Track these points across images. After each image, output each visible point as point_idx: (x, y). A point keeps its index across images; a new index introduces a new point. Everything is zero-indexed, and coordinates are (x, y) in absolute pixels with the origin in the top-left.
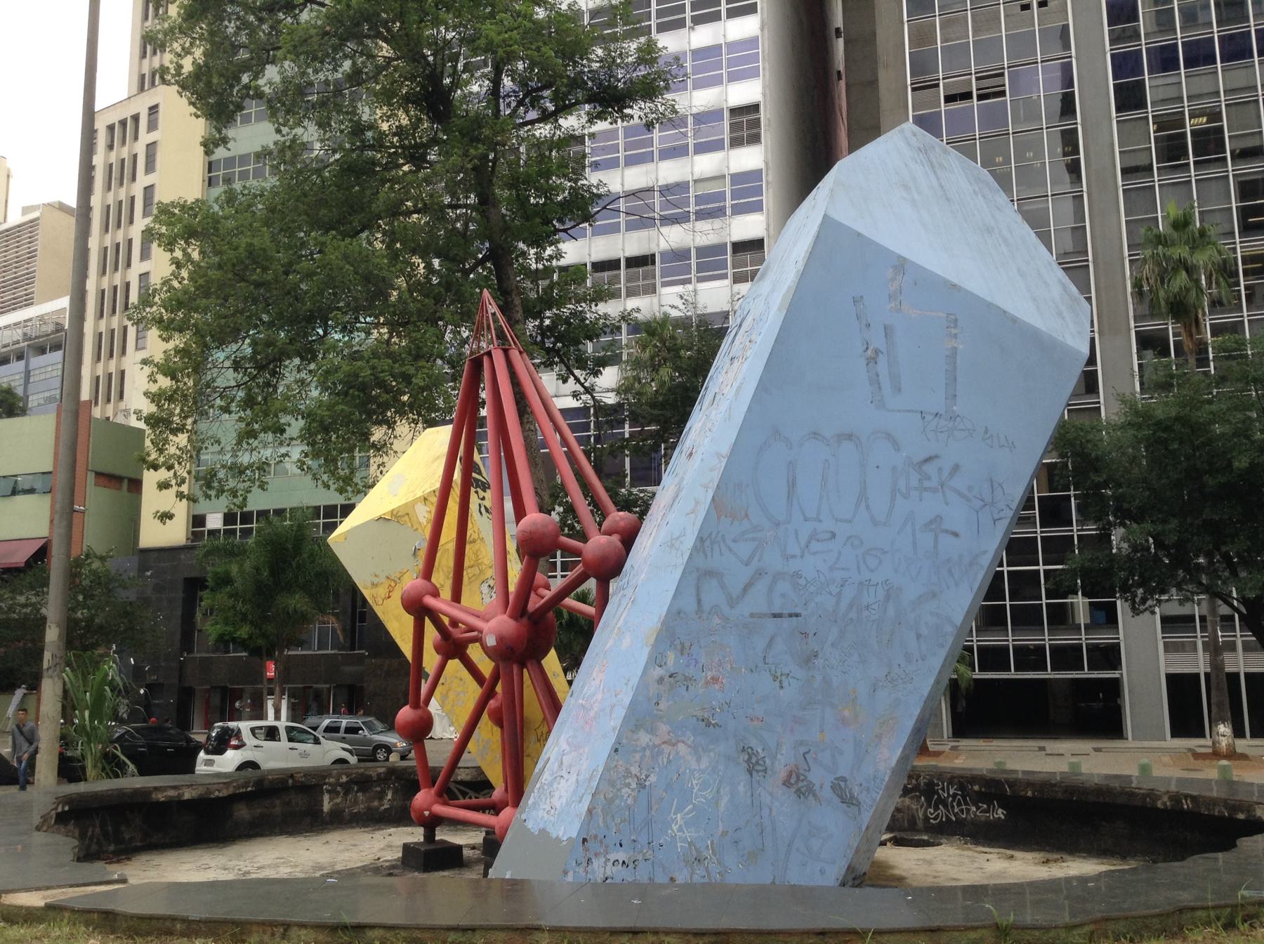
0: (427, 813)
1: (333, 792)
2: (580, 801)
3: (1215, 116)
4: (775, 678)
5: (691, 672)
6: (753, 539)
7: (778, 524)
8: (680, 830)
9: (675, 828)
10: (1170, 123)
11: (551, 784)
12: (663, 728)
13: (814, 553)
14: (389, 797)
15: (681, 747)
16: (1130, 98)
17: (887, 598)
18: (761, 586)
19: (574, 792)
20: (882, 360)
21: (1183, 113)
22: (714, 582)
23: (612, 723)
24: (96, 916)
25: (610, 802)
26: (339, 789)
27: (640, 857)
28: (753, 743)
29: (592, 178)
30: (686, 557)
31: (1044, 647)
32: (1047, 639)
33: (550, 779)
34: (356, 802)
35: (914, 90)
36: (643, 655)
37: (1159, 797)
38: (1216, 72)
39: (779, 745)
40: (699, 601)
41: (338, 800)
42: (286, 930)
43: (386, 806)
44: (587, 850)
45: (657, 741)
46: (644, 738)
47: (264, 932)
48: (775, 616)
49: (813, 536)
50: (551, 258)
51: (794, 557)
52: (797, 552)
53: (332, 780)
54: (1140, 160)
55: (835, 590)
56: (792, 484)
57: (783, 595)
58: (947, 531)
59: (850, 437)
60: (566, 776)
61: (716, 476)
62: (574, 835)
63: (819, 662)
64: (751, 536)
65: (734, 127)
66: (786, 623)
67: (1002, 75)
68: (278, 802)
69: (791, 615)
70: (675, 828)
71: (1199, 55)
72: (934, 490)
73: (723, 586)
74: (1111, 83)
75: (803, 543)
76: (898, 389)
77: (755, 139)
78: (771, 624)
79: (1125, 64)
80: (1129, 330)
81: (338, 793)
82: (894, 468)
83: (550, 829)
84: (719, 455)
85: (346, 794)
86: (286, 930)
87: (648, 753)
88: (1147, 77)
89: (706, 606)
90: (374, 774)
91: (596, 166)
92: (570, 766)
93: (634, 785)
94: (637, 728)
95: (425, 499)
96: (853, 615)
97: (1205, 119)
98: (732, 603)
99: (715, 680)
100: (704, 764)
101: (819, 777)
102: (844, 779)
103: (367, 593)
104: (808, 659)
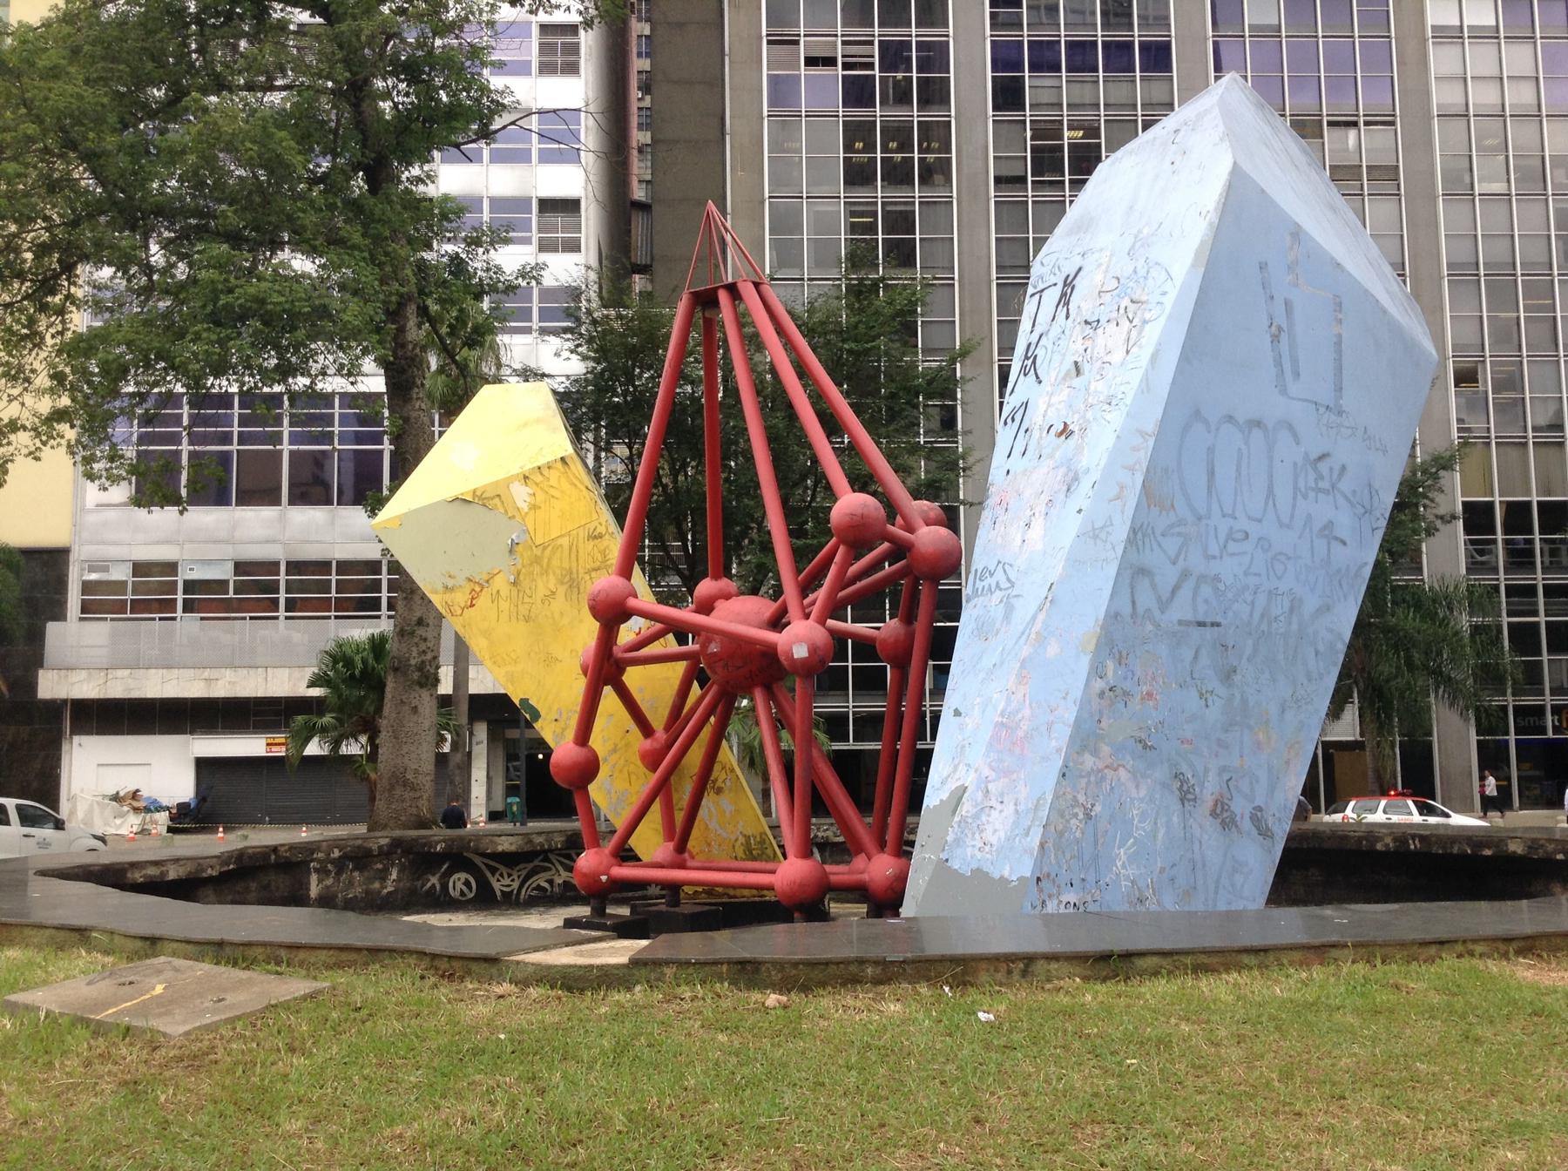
0: (604, 878)
1: (323, 872)
2: (1027, 834)
3: (1093, 131)
4: (1201, 695)
5: (1127, 686)
6: (1179, 534)
7: (1199, 519)
8: (1124, 866)
9: (1119, 864)
11: (976, 816)
12: (1106, 750)
13: (1233, 554)
14: (394, 876)
15: (1122, 771)
16: (1008, 96)
17: (1292, 610)
18: (1186, 592)
19: (1016, 824)
20: (1284, 337)
22: (1146, 582)
23: (1054, 743)
24: (725, 968)
25: (1061, 834)
26: (330, 866)
27: (1089, 898)
28: (1184, 768)
29: (496, 82)
30: (1120, 551)
34: (351, 883)
35: (769, 42)
36: (1084, 663)
37: (1380, 839)
38: (1134, 81)
39: (1206, 770)
40: (1134, 603)
41: (329, 882)
42: (1027, 966)
43: (390, 889)
44: (1041, 891)
45: (1101, 766)
46: (1089, 761)
47: (997, 970)
48: (1201, 624)
49: (1230, 537)
50: (419, 180)
51: (1214, 557)
52: (1217, 554)
53: (320, 855)
55: (1249, 599)
56: (1211, 473)
57: (1206, 601)
58: (1336, 538)
59: (1258, 424)
60: (999, 806)
61: (1144, 456)
62: (1028, 874)
63: (1237, 678)
64: (1177, 530)
65: (545, 48)
66: (1209, 633)
67: (871, 43)
68: (253, 885)
69: (1213, 624)
70: (1119, 864)
71: (1081, 56)
72: (1326, 492)
73: (1153, 586)
74: (989, 74)
75: (1222, 541)
76: (1297, 375)
77: (572, 69)
78: (1196, 632)
79: (1006, 58)
80: (992, 363)
81: (328, 873)
82: (1295, 464)
83: (987, 868)
84: (1143, 434)
85: (339, 873)
86: (1027, 966)
87: (1092, 779)
88: (1027, 74)
89: (1140, 610)
90: (375, 847)
91: (500, 67)
92: (1002, 795)
93: (1081, 816)
94: (1084, 748)
95: (526, 478)
96: (1264, 627)
97: (1081, 133)
98: (1164, 606)
99: (1150, 695)
100: (1143, 793)
101: (1241, 807)
102: (1260, 809)
104: (1228, 675)
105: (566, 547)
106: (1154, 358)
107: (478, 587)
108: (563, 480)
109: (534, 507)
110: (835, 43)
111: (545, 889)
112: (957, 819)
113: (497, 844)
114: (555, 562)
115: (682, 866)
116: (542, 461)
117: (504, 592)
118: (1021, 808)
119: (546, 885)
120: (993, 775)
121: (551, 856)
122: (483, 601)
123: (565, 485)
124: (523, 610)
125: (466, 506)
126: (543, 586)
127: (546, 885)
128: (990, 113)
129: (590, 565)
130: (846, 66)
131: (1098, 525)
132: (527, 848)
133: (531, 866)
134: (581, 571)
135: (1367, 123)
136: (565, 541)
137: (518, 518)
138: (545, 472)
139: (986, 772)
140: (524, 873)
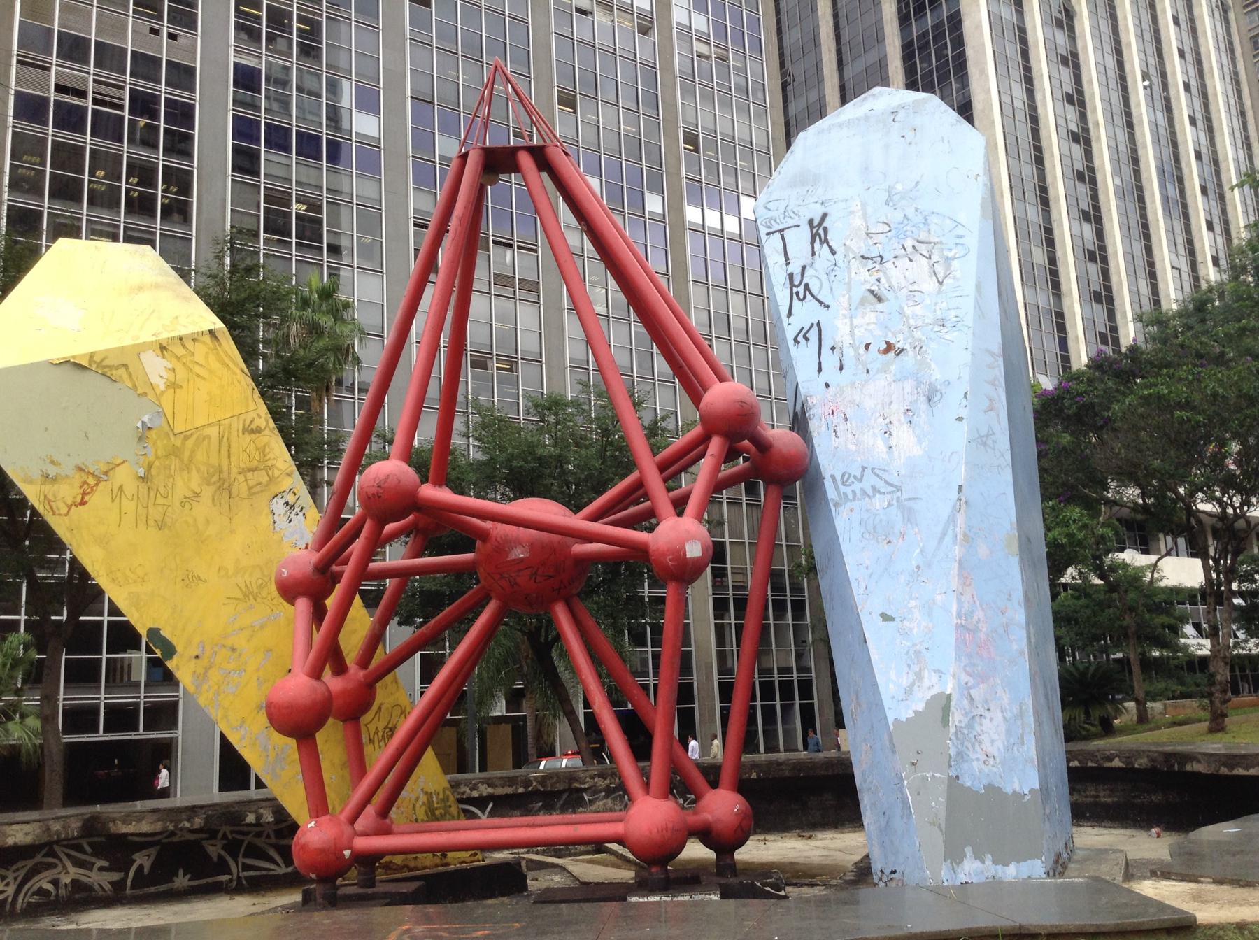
2: (1023, 743)
10: (278, 199)
16: (246, 162)
21: (290, 194)
23: (1015, 647)
31: (97, 707)
32: (102, 697)
33: (965, 720)
35: (19, 62)
54: (248, 224)
60: (986, 714)
74: (230, 141)
79: (245, 129)
83: (997, 782)
92: (986, 701)
95: (163, 348)
103: (32, 493)
105: (215, 441)
106: (978, 287)
107: (91, 481)
108: (212, 357)
109: (173, 385)
110: (86, 80)
111: (47, 893)
112: (952, 730)
113: (5, 835)
114: (200, 456)
115: (387, 831)
116: (182, 332)
117: (131, 487)
118: (1009, 715)
119: (50, 887)
120: (971, 681)
121: (57, 848)
122: (98, 499)
123: (215, 365)
124: (155, 513)
125: (78, 374)
126: (183, 485)
127: (50, 887)
128: (230, 172)
129: (245, 464)
130: (95, 101)
131: (983, 433)
132: (45, 839)
133: (30, 863)
134: (234, 470)
135: (519, 247)
136: (213, 432)
137: (151, 396)
138: (190, 344)
139: (964, 678)
140: (22, 874)
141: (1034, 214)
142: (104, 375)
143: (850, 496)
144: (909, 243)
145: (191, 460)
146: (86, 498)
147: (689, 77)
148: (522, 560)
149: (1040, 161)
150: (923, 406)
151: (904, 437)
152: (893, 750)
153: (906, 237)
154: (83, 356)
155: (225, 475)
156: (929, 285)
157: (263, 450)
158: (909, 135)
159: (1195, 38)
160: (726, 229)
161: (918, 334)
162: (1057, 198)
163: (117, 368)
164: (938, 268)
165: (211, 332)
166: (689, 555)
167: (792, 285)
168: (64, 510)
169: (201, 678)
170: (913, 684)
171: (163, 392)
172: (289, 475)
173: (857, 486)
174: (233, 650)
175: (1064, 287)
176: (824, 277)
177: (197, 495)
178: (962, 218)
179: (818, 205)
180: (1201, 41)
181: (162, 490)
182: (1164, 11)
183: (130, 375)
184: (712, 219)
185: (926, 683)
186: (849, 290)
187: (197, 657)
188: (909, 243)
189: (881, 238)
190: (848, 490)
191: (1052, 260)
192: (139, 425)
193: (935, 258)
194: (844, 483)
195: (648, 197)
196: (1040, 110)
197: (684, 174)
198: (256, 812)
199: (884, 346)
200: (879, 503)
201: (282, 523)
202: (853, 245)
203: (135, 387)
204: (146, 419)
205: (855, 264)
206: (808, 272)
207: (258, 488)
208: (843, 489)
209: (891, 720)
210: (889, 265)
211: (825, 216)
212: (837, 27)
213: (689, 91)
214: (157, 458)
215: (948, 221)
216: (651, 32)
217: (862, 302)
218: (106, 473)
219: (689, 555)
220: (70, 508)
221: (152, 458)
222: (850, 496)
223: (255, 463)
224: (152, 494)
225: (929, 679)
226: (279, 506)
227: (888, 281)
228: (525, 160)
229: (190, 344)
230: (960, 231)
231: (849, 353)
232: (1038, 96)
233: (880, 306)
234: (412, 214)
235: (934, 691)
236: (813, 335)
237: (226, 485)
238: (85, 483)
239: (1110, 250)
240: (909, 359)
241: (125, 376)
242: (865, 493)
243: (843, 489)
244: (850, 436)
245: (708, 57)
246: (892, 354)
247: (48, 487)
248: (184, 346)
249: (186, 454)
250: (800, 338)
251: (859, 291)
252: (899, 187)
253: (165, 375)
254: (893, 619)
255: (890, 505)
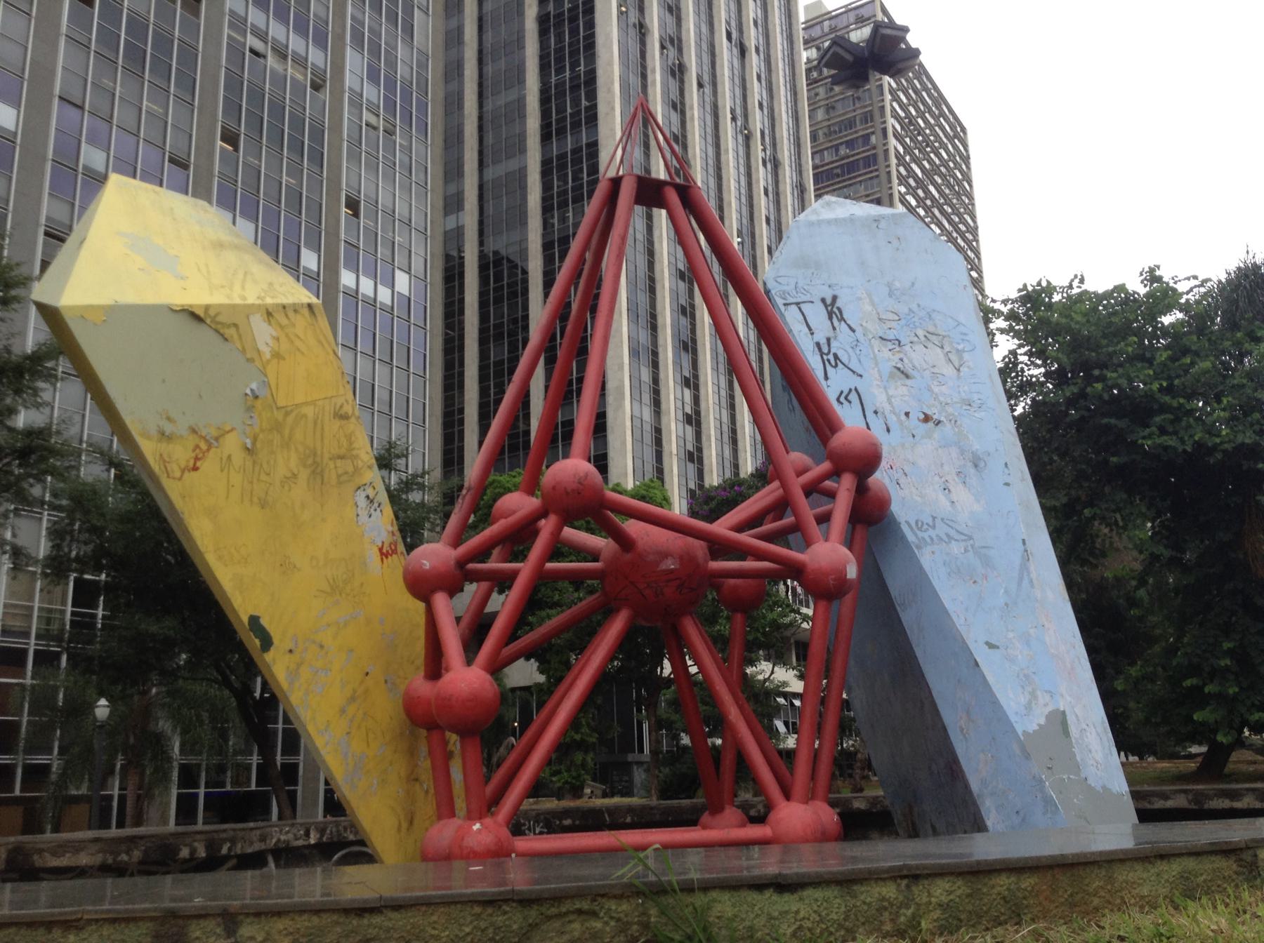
107: (205, 444)
109: (277, 355)
117: (238, 457)
122: (209, 465)
134: (327, 456)
137: (258, 363)
138: (291, 314)
141: (644, 337)
142: (217, 331)
143: (928, 540)
144: (921, 333)
145: (290, 438)
146: (198, 464)
147: (356, 143)
148: (672, 571)
149: (652, 290)
150: (972, 471)
151: (961, 494)
152: (1027, 756)
153: (916, 327)
154: (199, 306)
155: (318, 459)
156: (949, 371)
157: (350, 437)
158: (895, 242)
159: (778, 209)
160: (379, 299)
161: (950, 410)
162: (665, 325)
163: (229, 326)
164: (953, 357)
165: (310, 306)
166: (849, 576)
167: (822, 354)
168: (178, 474)
169: (294, 674)
170: (1030, 702)
171: (268, 361)
172: (370, 467)
173: (931, 532)
174: (322, 647)
175: (663, 406)
176: (850, 350)
177: (295, 476)
178: (962, 319)
179: (826, 288)
180: (783, 212)
181: (265, 466)
182: (758, 181)
183: (240, 337)
184: (366, 286)
185: (1041, 701)
186: (877, 364)
187: (291, 651)
188: (921, 333)
189: (894, 324)
190: (926, 535)
191: (656, 380)
192: (248, 392)
193: (947, 348)
194: (920, 529)
195: (304, 251)
196: (656, 245)
197: (343, 236)
198: (190, 845)
199: (922, 416)
200: (956, 549)
201: (363, 517)
202: (869, 326)
203: (244, 351)
204: (254, 386)
205: (876, 344)
206: (834, 344)
207: (345, 478)
208: (920, 534)
209: (1020, 733)
210: (907, 348)
211: (835, 298)
212: (481, 128)
213: (354, 156)
214: (262, 430)
215: (950, 320)
216: (322, 90)
217: (891, 376)
218: (217, 439)
219: (849, 576)
220: (183, 471)
221: (257, 430)
222: (928, 540)
223: (343, 451)
224: (257, 468)
225: (1043, 698)
226: (362, 502)
227: (911, 361)
228: (673, 197)
229: (291, 314)
230: (962, 329)
231: (892, 420)
232: (656, 233)
233: (908, 382)
234: (43, 221)
235: (1050, 708)
236: (853, 397)
237: (319, 470)
238: (197, 447)
239: (702, 379)
240: (947, 428)
241: (236, 336)
242: (941, 539)
243: (920, 534)
244: (914, 490)
245: (375, 128)
246: (931, 424)
247: (164, 445)
248: (287, 315)
249: (287, 432)
250: (842, 399)
251: (887, 368)
252: (897, 284)
253: (271, 342)
254: (998, 647)
255: (966, 551)
